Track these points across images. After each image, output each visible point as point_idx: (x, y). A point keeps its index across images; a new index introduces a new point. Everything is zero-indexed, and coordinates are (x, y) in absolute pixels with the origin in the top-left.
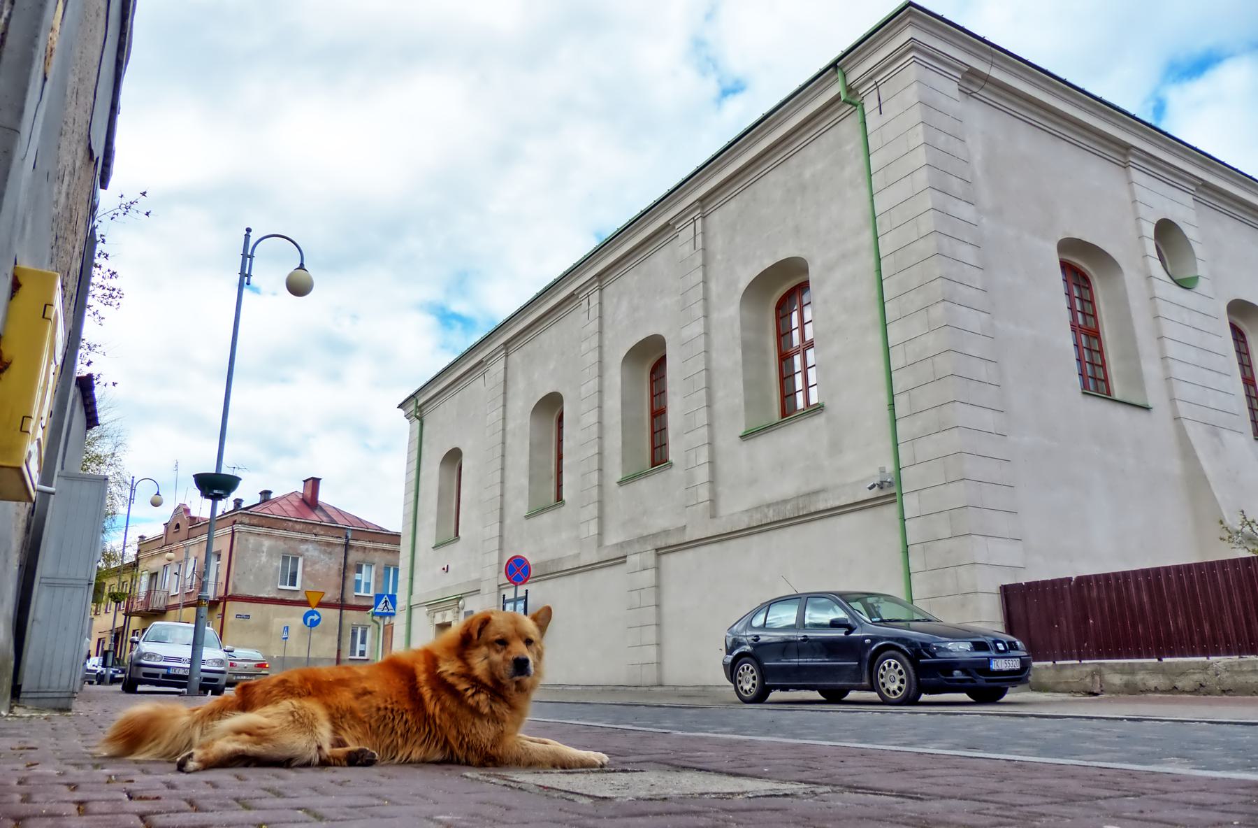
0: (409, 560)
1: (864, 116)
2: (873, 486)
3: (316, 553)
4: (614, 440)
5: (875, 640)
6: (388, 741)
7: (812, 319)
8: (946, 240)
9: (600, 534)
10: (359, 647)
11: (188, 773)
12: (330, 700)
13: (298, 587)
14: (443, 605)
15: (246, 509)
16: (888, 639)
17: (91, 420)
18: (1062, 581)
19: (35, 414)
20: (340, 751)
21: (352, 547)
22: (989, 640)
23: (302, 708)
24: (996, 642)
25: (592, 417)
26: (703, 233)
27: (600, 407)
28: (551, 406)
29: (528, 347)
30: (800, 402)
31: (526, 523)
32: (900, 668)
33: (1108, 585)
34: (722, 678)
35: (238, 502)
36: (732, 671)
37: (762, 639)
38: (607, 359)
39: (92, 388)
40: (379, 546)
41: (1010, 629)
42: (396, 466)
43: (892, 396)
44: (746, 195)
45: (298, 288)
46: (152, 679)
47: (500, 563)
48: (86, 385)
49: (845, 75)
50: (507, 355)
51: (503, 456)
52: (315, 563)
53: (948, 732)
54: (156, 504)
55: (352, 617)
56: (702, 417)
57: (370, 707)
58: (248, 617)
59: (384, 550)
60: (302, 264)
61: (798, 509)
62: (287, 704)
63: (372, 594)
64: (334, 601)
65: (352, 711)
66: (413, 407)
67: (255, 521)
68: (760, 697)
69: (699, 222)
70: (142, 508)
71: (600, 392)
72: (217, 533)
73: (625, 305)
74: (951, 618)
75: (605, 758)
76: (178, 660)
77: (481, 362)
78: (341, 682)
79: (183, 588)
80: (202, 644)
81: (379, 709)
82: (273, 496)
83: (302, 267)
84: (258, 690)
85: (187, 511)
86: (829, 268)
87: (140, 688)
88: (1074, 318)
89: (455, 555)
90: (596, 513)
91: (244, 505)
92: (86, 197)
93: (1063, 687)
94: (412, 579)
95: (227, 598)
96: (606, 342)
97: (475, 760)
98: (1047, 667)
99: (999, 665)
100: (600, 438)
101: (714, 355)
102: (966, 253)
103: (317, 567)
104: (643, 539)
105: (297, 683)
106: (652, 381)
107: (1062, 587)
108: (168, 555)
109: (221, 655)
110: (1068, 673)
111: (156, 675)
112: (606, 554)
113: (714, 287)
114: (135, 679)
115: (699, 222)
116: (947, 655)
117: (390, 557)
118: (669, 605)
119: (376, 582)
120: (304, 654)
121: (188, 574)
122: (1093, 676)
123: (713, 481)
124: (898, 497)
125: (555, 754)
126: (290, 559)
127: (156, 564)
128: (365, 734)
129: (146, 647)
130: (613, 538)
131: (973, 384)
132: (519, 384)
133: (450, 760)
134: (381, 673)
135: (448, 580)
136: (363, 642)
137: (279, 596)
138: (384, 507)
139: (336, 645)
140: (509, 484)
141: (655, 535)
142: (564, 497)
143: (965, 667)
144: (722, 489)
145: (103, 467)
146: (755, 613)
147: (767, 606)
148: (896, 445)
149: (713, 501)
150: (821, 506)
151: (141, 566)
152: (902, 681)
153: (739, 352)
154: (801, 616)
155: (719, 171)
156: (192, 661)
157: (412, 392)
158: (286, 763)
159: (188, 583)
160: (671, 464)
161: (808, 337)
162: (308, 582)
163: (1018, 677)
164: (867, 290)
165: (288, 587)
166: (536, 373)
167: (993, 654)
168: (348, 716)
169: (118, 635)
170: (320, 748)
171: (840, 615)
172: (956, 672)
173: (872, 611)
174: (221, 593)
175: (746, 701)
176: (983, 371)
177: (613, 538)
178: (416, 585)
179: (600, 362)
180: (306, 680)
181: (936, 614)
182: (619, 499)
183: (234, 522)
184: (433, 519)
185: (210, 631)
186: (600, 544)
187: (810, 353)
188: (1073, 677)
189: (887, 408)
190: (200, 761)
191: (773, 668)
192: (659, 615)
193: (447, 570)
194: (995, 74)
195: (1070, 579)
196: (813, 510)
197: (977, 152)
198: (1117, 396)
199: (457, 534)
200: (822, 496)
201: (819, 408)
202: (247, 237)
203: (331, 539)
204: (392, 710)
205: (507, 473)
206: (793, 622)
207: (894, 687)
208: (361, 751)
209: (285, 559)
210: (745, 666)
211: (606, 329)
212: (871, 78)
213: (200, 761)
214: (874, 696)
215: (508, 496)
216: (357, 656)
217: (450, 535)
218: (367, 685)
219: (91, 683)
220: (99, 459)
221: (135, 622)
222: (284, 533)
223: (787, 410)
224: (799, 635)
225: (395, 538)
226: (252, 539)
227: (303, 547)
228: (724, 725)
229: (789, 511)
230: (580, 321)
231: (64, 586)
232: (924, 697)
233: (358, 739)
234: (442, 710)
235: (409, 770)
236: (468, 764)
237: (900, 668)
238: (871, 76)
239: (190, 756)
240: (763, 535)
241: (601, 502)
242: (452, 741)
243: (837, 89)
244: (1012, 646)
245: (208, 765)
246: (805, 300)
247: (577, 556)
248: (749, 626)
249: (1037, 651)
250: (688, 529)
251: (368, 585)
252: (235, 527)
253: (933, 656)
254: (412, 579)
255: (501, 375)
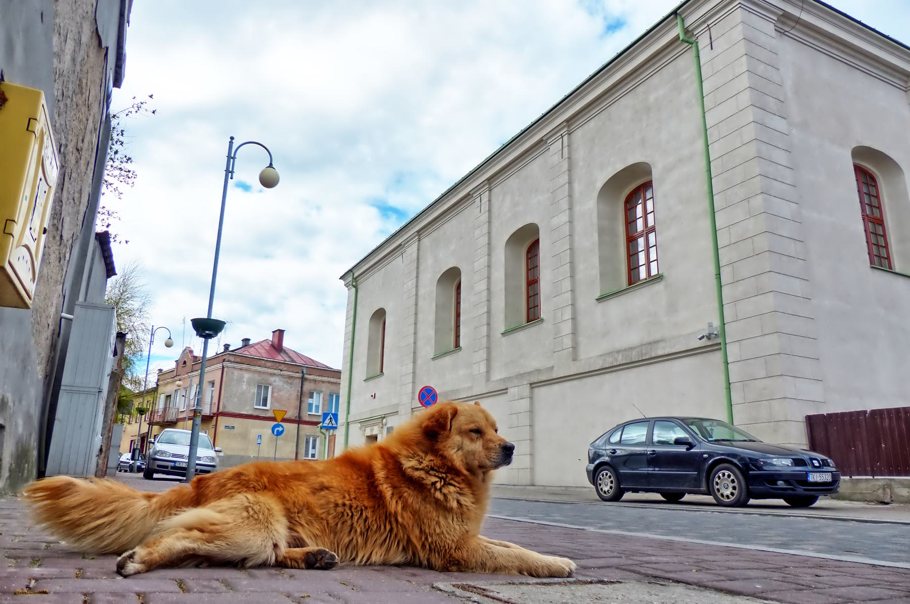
0: (347, 389)
1: (698, 51)
2: (703, 337)
3: (281, 384)
4: (499, 302)
5: (711, 455)
6: (347, 540)
7: (653, 209)
8: (764, 147)
9: (488, 372)
10: (311, 451)
11: (125, 577)
12: (285, 494)
13: (268, 407)
14: (371, 422)
15: (233, 351)
16: (722, 454)
17: (110, 271)
18: (858, 413)
19: (20, 217)
20: (298, 552)
21: (306, 379)
22: (806, 458)
23: (258, 503)
24: (812, 459)
25: (483, 286)
26: (569, 146)
27: (489, 278)
28: (452, 277)
29: (435, 234)
30: (643, 274)
31: (433, 363)
32: (732, 477)
33: (898, 418)
34: (586, 481)
35: (227, 347)
36: (594, 476)
37: (619, 453)
38: (494, 242)
39: (109, 242)
40: (325, 379)
41: (813, 447)
42: (340, 321)
43: (718, 267)
44: (604, 115)
45: (268, 182)
46: (163, 469)
47: (413, 393)
48: (104, 239)
49: (683, 20)
50: (419, 240)
51: (416, 314)
52: (280, 390)
53: (768, 530)
54: (168, 345)
55: (306, 429)
56: (567, 285)
57: (328, 503)
58: (233, 427)
59: (329, 382)
60: (271, 164)
61: (642, 354)
62: (242, 498)
63: (320, 413)
64: (293, 418)
65: (309, 507)
66: (350, 279)
67: (238, 360)
68: (616, 497)
69: (565, 138)
70: (158, 348)
71: (489, 266)
72: (206, 369)
73: (508, 199)
74: (769, 439)
75: (573, 565)
76: (182, 456)
77: (400, 245)
78: (298, 477)
79: (188, 406)
80: (197, 445)
81: (337, 505)
82: (251, 342)
83: (271, 165)
84: (213, 483)
85: (191, 352)
86: (669, 170)
87: (155, 476)
88: (863, 210)
89: (380, 386)
90: (485, 356)
91: (231, 349)
92: (98, 81)
93: (859, 496)
94: (349, 403)
95: (219, 414)
96: (494, 230)
97: (437, 561)
98: (844, 481)
99: (814, 477)
100: (489, 301)
101: (576, 238)
102: (780, 156)
103: (282, 393)
104: (521, 376)
105: (252, 477)
106: (528, 259)
107: (858, 419)
108: (178, 383)
109: (212, 453)
110: (863, 486)
111: (167, 467)
112: (492, 387)
113: (577, 187)
114: (151, 469)
115: (565, 138)
116: (772, 468)
117: (333, 387)
118: (539, 426)
119: (323, 404)
120: (272, 455)
121: (192, 396)
122: (884, 489)
123: (575, 333)
124: (722, 346)
125: (519, 558)
126: (263, 387)
127: (169, 389)
128: (323, 531)
129: (159, 447)
130: (497, 375)
131: (785, 258)
132: (428, 261)
133: (412, 564)
134: (338, 469)
135: (376, 403)
136: (314, 447)
137: (255, 414)
138: (331, 355)
139: (295, 449)
140: (420, 334)
141: (529, 373)
142: (461, 344)
143: (789, 478)
144: (582, 339)
145: (133, 319)
146: (614, 430)
147: (623, 427)
148: (722, 306)
149: (575, 348)
150: (660, 353)
151: (160, 390)
152: (734, 488)
153: (596, 236)
154: (650, 435)
155: (582, 98)
156: (189, 457)
157: (350, 268)
158: (238, 564)
159: (192, 403)
160: (542, 320)
161: (651, 223)
162: (276, 404)
163: (829, 488)
164: (699, 187)
165: (261, 407)
166: (441, 253)
167: (810, 468)
168: (305, 512)
169: (144, 438)
170: (276, 546)
171: (681, 434)
172: (780, 482)
173: (703, 431)
174: (215, 410)
175: (605, 500)
176: (792, 248)
177: (498, 375)
178: (352, 407)
179: (489, 244)
180: (261, 473)
181: (754, 434)
182: (503, 346)
183: (224, 360)
184: (364, 360)
185: (203, 436)
186: (488, 379)
187: (652, 236)
188: (867, 489)
189: (714, 277)
190: (143, 562)
191: (627, 474)
192: (532, 433)
193: (374, 396)
194: (805, 17)
195: (865, 412)
196: (653, 355)
197: (788, 77)
198: (897, 271)
199: (382, 371)
200: (661, 345)
201: (659, 278)
202: (231, 143)
203: (292, 374)
204: (351, 507)
205: (418, 326)
206: (643, 439)
207: (727, 492)
208: (320, 552)
209: (259, 387)
210: (604, 472)
211: (494, 220)
212: (704, 22)
213: (143, 562)
214: (709, 499)
215: (420, 343)
216: (310, 458)
217: (377, 371)
218: (325, 480)
219: (126, 471)
220: (129, 313)
221: (156, 428)
222: (259, 369)
223: (633, 279)
224: (649, 450)
225: (337, 374)
226: (236, 373)
227: (272, 379)
228: (607, 520)
229: (634, 356)
230: (474, 213)
231: (79, 392)
232: (752, 501)
233: (316, 536)
234: (403, 508)
235: (369, 574)
236: (430, 567)
237: (732, 477)
238: (704, 20)
239: (131, 557)
240: (614, 374)
241: (489, 349)
242: (414, 540)
243: (677, 31)
244: (824, 463)
245: (152, 566)
246: (649, 195)
247: (471, 388)
248: (608, 442)
249: (844, 468)
250: (555, 369)
251: (317, 407)
252: (225, 363)
253: (759, 468)
254: (349, 403)
255: (415, 255)
